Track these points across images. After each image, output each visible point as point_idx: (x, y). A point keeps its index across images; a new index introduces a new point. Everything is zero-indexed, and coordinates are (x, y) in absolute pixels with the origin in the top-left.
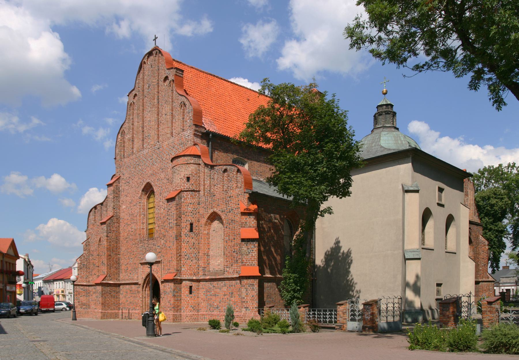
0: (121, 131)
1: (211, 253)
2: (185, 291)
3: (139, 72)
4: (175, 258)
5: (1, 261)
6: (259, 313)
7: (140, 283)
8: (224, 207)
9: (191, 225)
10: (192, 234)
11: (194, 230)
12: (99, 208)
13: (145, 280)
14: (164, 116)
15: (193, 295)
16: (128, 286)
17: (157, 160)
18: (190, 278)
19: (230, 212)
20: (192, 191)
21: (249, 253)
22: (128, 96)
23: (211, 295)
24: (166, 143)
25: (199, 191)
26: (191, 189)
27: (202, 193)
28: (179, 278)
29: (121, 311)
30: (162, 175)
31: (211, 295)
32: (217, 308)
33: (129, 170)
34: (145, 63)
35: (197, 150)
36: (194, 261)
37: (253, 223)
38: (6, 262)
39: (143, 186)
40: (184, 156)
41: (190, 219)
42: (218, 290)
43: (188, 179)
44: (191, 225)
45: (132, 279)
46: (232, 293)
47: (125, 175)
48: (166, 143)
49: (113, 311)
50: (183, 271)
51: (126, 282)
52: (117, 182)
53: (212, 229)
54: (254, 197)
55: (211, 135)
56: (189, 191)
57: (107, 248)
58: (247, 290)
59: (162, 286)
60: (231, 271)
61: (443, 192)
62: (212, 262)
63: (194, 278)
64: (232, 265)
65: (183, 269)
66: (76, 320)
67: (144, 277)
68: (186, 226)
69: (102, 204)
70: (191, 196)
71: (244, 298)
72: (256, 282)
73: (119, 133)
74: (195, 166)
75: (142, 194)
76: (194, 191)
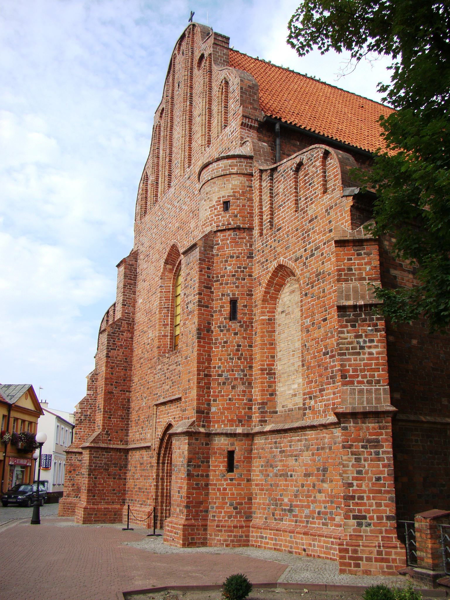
2: (217, 465)
3: (169, 72)
4: (195, 381)
5: (4, 416)
6: (401, 538)
9: (233, 303)
10: (235, 325)
11: (239, 316)
13: (162, 440)
15: (235, 474)
18: (229, 429)
19: (312, 255)
20: (234, 229)
21: (362, 348)
26: (233, 224)
27: (256, 232)
29: (126, 507)
31: (276, 475)
32: (290, 511)
35: (247, 150)
36: (241, 388)
37: (368, 268)
38: (16, 419)
41: (230, 291)
42: (291, 462)
43: (226, 205)
46: (325, 470)
50: (214, 413)
53: (279, 310)
55: (277, 127)
56: (229, 229)
57: (106, 379)
58: (358, 460)
60: (319, 406)
63: (239, 430)
64: (321, 390)
65: (213, 409)
68: (222, 307)
70: (233, 240)
71: (351, 485)
74: (242, 178)
75: (165, 269)
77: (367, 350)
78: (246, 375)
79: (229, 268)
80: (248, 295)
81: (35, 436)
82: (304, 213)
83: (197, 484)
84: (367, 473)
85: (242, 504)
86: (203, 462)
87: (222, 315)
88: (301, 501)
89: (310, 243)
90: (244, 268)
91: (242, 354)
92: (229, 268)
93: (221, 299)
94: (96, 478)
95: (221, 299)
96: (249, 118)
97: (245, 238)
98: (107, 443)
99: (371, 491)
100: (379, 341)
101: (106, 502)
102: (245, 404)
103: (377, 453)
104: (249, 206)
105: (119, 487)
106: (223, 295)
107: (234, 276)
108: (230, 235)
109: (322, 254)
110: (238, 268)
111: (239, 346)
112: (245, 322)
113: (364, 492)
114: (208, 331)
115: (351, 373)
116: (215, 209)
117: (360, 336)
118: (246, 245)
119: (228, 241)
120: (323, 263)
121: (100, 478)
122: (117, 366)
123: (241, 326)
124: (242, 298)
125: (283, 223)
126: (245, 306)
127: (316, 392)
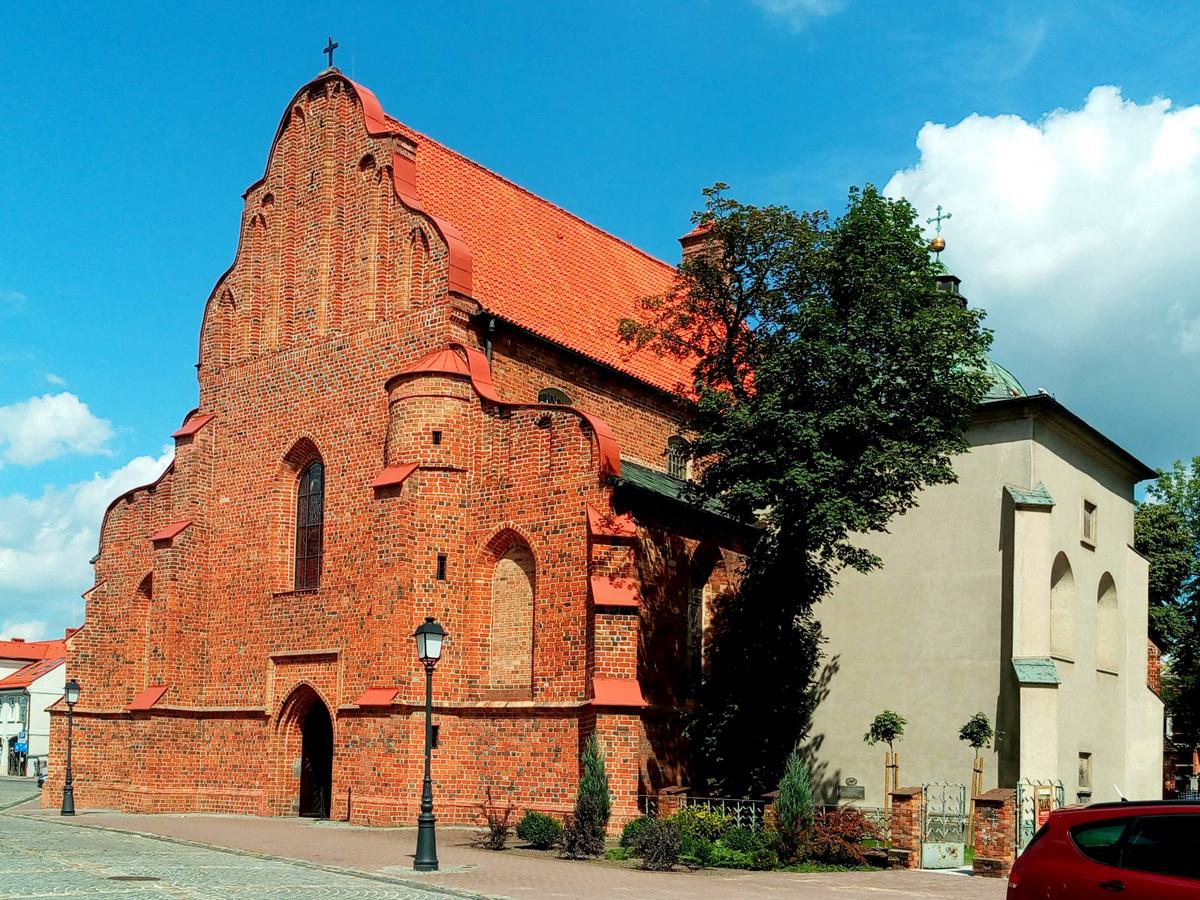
0: (222, 292)
1: (492, 639)
7: (268, 713)
8: (537, 517)
9: (442, 559)
10: (444, 587)
12: (139, 498)
13: (285, 705)
14: (358, 261)
16: (227, 722)
17: (335, 380)
19: (556, 532)
20: (445, 469)
22: (245, 197)
23: (493, 754)
24: (365, 335)
25: (464, 471)
28: (404, 702)
30: (350, 423)
33: (243, 399)
34: (299, 112)
39: (288, 447)
40: (428, 374)
42: (516, 741)
43: (437, 437)
44: (442, 559)
45: (244, 702)
46: (558, 750)
47: (233, 410)
48: (365, 335)
49: (180, 791)
51: (228, 709)
52: (205, 429)
54: (627, 497)
55: (492, 324)
56: (439, 469)
58: (609, 744)
59: (338, 726)
61: (1094, 512)
62: (495, 662)
63: (446, 704)
64: (559, 674)
66: (72, 812)
67: (283, 697)
69: (151, 488)
70: (444, 483)
72: (572, 726)
73: (213, 296)
74: (457, 402)
76: (450, 469)
77: (619, 646)
78: (453, 644)
79: (437, 516)
80: (459, 551)
81: (813, 707)
82: (548, 480)
83: (398, 761)
84: (616, 755)
85: (446, 782)
86: (403, 737)
87: (428, 572)
88: (525, 779)
89: (553, 517)
90: (456, 518)
91: (450, 620)
92: (437, 516)
93: (427, 553)
94: (160, 752)
95: (427, 553)
96: (461, 311)
97: (458, 482)
98: (174, 704)
99: (618, 771)
100: (630, 639)
101: (175, 785)
102: (452, 676)
103: (626, 739)
104: (463, 441)
105: (191, 765)
106: (429, 548)
107: (443, 527)
108: (439, 475)
109: (570, 535)
110: (449, 517)
111: (447, 610)
112: (455, 583)
113: (613, 771)
114: (411, 590)
115: (604, 666)
116: (422, 438)
117: (615, 633)
118: (458, 490)
119: (437, 483)
120: (570, 545)
121: (165, 753)
122: (188, 594)
123: (450, 588)
124: (451, 556)
125: (516, 481)
126: (455, 565)
127: (551, 674)
